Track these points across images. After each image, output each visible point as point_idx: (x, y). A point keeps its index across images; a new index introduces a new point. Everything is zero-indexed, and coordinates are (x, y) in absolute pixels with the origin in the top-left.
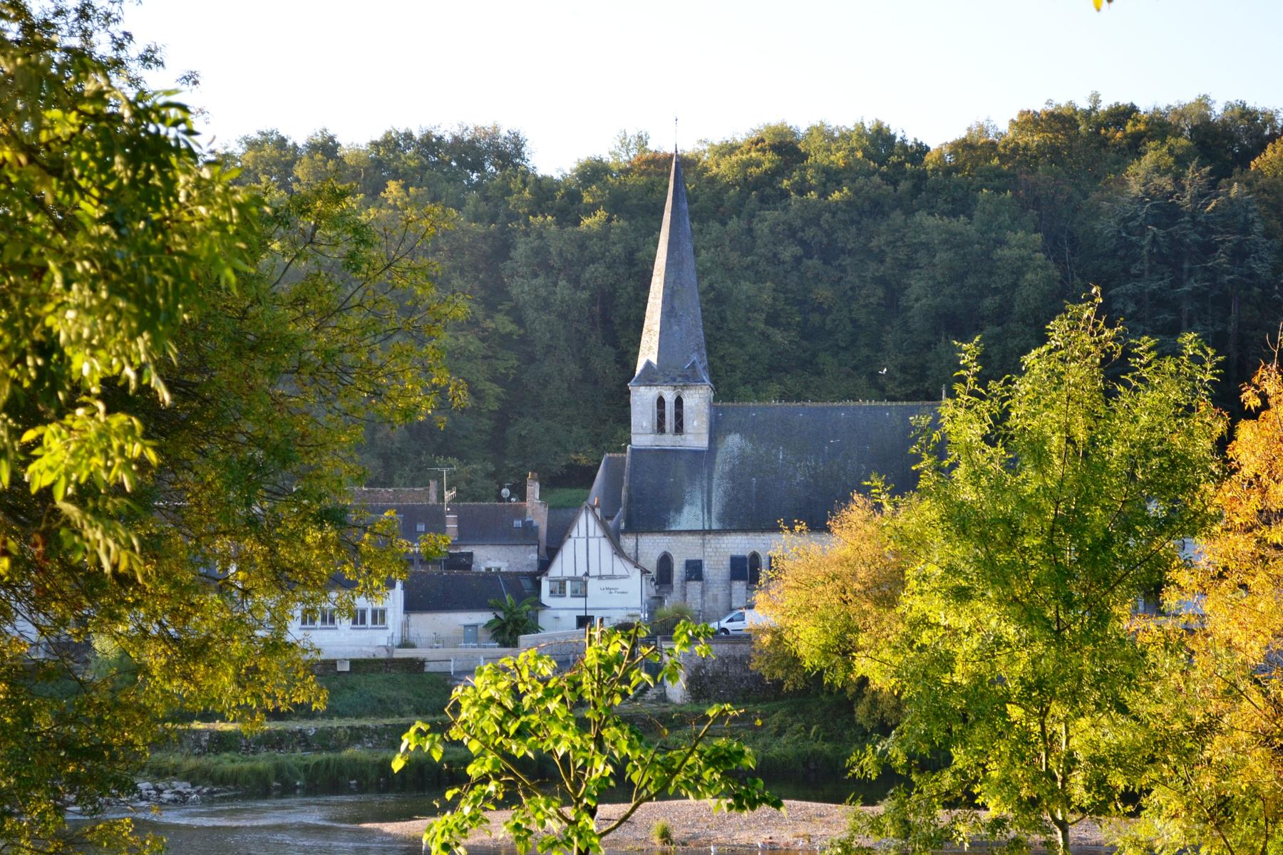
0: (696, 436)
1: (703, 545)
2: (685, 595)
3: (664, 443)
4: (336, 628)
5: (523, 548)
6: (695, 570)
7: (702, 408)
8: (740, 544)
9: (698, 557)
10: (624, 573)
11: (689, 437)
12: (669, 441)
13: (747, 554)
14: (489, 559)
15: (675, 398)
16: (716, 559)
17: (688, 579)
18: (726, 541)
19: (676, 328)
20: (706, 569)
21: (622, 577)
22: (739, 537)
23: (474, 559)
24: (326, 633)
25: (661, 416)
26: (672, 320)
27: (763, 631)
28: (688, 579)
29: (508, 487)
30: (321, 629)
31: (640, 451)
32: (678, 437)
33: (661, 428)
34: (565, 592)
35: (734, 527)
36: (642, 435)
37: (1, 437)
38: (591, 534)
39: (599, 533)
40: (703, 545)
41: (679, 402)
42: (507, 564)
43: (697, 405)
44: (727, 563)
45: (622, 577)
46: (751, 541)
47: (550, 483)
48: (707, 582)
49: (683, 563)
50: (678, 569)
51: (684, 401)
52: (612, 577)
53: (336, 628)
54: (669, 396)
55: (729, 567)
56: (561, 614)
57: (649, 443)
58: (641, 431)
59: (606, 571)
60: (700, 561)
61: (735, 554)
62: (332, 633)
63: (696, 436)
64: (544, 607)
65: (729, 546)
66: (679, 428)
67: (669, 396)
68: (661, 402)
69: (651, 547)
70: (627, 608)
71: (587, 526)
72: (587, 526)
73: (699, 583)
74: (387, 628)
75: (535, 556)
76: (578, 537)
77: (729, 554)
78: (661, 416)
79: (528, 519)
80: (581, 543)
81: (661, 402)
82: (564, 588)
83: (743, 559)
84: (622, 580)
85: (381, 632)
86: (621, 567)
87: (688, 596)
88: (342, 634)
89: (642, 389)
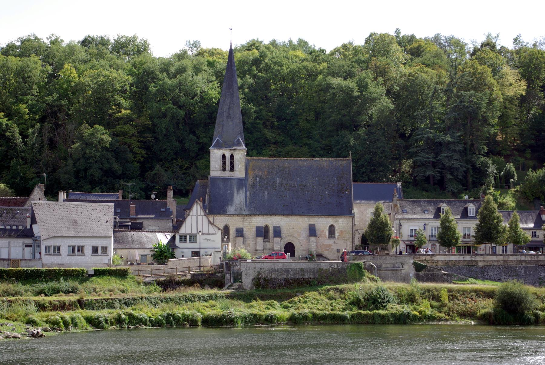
0: (240, 172)
1: (244, 221)
2: (236, 244)
3: (225, 175)
4: (85, 255)
5: (165, 220)
6: (240, 233)
7: (243, 159)
8: (260, 221)
9: (241, 226)
10: (214, 232)
11: (236, 173)
12: (227, 174)
13: (264, 225)
14: (150, 225)
15: (230, 155)
16: (249, 227)
17: (237, 236)
18: (254, 220)
19: (231, 123)
20: (245, 232)
21: (213, 234)
22: (260, 218)
23: (143, 225)
24: (80, 257)
25: (224, 163)
26: (229, 120)
27: (188, 328)
28: (237, 236)
29: (154, 194)
30: (77, 255)
31: (212, 178)
32: (232, 173)
33: (224, 169)
34: (186, 241)
35: (258, 213)
36: (215, 170)
37: (544, 186)
38: (199, 214)
39: (203, 214)
40: (244, 221)
41: (232, 157)
42: (158, 228)
43: (240, 158)
44: (254, 229)
45: (213, 234)
46: (265, 220)
47: (178, 194)
48: (245, 238)
49: (234, 229)
50: (232, 232)
51: (234, 156)
52: (208, 234)
53: (85, 255)
54: (228, 154)
55: (255, 231)
56: (185, 250)
57: (218, 175)
58: (214, 169)
59: (205, 231)
60: (242, 229)
61: (258, 225)
62: (83, 257)
63: (240, 172)
64: (177, 247)
65: (255, 221)
66: (232, 169)
67: (228, 154)
68: (224, 157)
69: (221, 221)
70: (215, 248)
71: (197, 211)
72: (197, 211)
73: (242, 238)
74: (108, 255)
75: (171, 224)
76: (193, 216)
77: (255, 226)
78: (224, 163)
79: (168, 208)
80: (194, 218)
81: (224, 157)
82: (186, 239)
83: (261, 227)
84: (213, 235)
85: (105, 257)
86: (212, 229)
87: (237, 244)
88: (87, 258)
89: (216, 151)
